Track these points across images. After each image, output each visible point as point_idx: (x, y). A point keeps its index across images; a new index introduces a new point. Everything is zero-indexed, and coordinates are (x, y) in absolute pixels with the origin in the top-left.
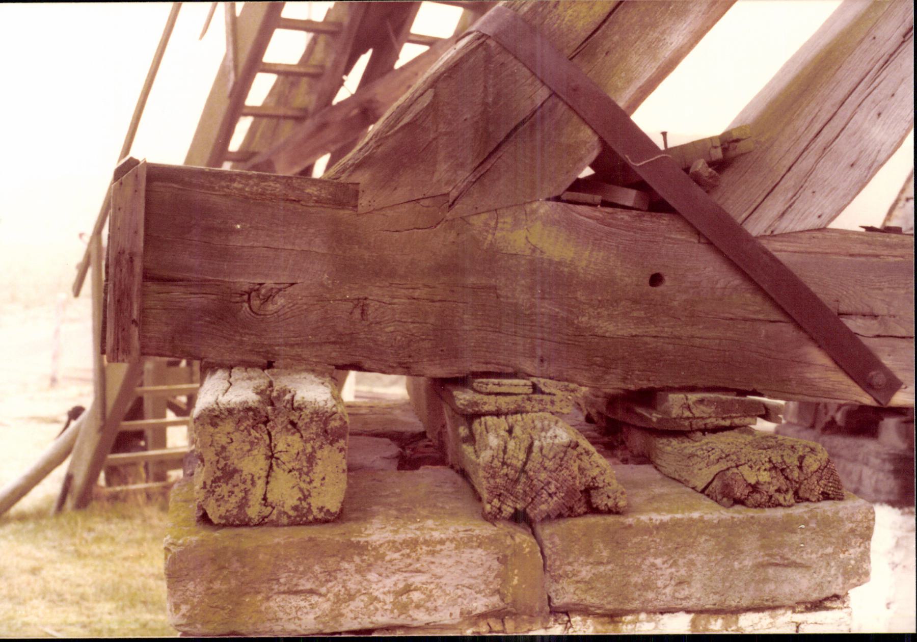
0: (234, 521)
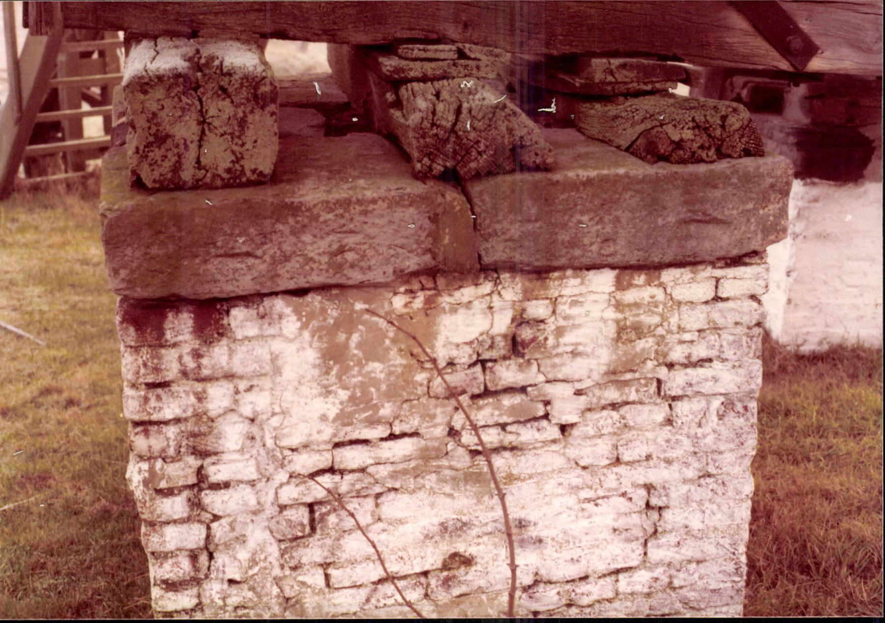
0: (168, 185)
